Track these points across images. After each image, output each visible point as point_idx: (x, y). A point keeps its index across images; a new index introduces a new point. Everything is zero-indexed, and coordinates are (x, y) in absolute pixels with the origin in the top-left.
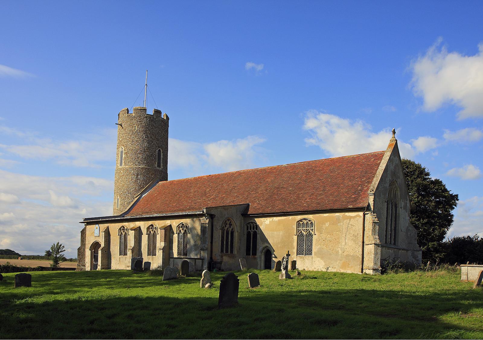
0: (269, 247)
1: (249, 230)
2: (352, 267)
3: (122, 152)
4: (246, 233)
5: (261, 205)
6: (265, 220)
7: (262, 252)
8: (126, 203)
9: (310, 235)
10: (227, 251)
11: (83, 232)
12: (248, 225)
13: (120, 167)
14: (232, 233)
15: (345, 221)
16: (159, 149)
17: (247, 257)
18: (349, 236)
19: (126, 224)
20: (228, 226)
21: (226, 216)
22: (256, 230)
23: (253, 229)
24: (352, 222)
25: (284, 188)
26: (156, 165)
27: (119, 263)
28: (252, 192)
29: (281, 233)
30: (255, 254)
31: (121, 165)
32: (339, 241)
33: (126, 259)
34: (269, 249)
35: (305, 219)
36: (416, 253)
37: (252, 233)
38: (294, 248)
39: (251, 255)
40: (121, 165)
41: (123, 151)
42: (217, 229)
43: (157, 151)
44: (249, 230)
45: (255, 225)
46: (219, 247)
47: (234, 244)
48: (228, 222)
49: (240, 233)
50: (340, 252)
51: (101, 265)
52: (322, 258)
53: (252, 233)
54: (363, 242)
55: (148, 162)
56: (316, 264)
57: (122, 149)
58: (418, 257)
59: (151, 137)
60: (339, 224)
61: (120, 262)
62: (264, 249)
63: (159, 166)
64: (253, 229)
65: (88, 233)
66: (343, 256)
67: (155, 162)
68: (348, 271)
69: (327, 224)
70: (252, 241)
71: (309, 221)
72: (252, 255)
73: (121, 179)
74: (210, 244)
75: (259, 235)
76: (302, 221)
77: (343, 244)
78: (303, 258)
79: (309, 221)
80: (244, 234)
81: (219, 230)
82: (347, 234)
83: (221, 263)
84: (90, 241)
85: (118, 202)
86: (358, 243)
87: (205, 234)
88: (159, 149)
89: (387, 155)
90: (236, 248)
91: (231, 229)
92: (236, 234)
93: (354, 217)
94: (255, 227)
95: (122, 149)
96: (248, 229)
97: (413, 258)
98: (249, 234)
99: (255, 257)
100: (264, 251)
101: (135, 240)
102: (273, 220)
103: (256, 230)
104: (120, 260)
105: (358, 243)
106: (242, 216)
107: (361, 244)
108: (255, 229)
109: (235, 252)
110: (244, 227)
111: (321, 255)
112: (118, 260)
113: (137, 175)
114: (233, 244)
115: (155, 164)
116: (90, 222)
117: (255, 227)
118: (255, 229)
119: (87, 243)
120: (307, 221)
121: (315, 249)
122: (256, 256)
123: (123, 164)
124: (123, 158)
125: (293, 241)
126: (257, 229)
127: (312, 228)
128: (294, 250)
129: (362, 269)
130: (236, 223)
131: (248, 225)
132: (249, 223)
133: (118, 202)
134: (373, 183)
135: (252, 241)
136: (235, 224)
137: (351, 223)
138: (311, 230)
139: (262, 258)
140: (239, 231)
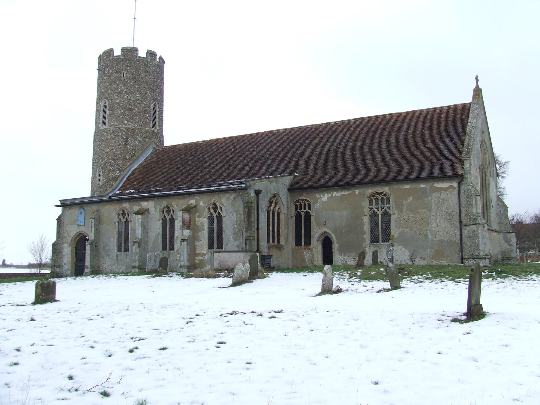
0: (329, 234)
1: (299, 210)
2: (448, 256)
3: (105, 108)
4: (294, 213)
5: (313, 176)
6: (322, 196)
7: (318, 240)
8: (111, 177)
9: (386, 215)
10: (273, 241)
11: (59, 220)
12: (297, 203)
13: (102, 128)
14: (279, 214)
15: (434, 195)
16: (154, 102)
17: (297, 247)
18: (441, 215)
19: (126, 205)
20: (273, 204)
21: (273, 192)
22: (308, 210)
23: (305, 209)
24: (444, 195)
25: (341, 153)
26: (151, 125)
27: (116, 262)
28: (296, 158)
29: (345, 213)
30: (308, 243)
31: (104, 124)
32: (428, 221)
33: (127, 256)
34: (329, 236)
35: (379, 193)
36: (509, 236)
37: (303, 214)
38: (365, 233)
39: (303, 244)
40: (104, 124)
41: (107, 106)
42: (262, 209)
43: (152, 105)
44: (299, 210)
45: (306, 203)
46: (266, 235)
47: (281, 230)
48: (274, 200)
49: (287, 214)
50: (430, 236)
51: (89, 266)
52: (405, 246)
53: (303, 214)
54: (461, 222)
55: (141, 121)
56: (397, 254)
57: (105, 103)
58: (511, 241)
59: (145, 87)
60: (426, 199)
61: (117, 262)
62: (321, 236)
63: (154, 126)
64: (305, 209)
65: (66, 220)
66: (435, 242)
67: (150, 121)
68: (443, 262)
69: (410, 199)
70: (303, 226)
71: (385, 195)
72: (305, 245)
73: (104, 144)
74: (256, 231)
75: (313, 216)
76: (374, 196)
77: (434, 225)
78: (379, 246)
79: (385, 195)
80: (292, 217)
81: (265, 211)
82: (438, 212)
83: (271, 258)
84: (72, 231)
85: (100, 176)
86: (454, 224)
87: (251, 216)
88: (154, 102)
89: (474, 107)
90: (283, 237)
91: (277, 208)
92: (282, 217)
93: (446, 189)
94: (307, 205)
95: (105, 103)
96: (296, 209)
97: (506, 242)
98: (298, 216)
99: (309, 248)
100: (320, 239)
101: (143, 228)
102: (332, 195)
103: (308, 210)
104: (117, 259)
105: (454, 224)
106: (289, 191)
107: (457, 224)
108: (307, 208)
109: (282, 242)
110: (291, 205)
111: (404, 242)
112: (115, 258)
113: (127, 138)
114: (280, 230)
115: (150, 123)
116: (66, 205)
117: (307, 205)
118: (307, 208)
119: (65, 235)
120: (381, 195)
121: (395, 232)
122: (311, 247)
123: (107, 123)
124: (107, 115)
125: (363, 223)
126: (309, 209)
127: (388, 206)
128: (365, 236)
129: (462, 259)
130: (282, 200)
131: (297, 203)
132: (298, 201)
133: (100, 176)
134: (466, 143)
135: (303, 226)
136: (281, 203)
137: (442, 197)
138: (376, 209)
139: (319, 249)
140: (286, 212)
